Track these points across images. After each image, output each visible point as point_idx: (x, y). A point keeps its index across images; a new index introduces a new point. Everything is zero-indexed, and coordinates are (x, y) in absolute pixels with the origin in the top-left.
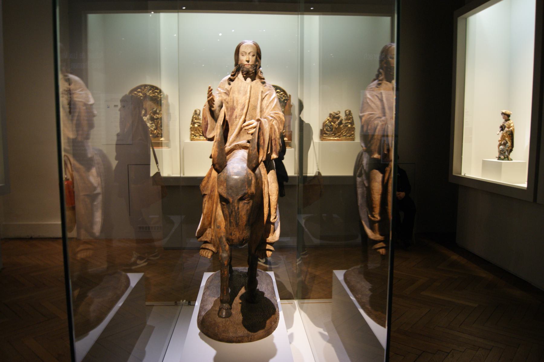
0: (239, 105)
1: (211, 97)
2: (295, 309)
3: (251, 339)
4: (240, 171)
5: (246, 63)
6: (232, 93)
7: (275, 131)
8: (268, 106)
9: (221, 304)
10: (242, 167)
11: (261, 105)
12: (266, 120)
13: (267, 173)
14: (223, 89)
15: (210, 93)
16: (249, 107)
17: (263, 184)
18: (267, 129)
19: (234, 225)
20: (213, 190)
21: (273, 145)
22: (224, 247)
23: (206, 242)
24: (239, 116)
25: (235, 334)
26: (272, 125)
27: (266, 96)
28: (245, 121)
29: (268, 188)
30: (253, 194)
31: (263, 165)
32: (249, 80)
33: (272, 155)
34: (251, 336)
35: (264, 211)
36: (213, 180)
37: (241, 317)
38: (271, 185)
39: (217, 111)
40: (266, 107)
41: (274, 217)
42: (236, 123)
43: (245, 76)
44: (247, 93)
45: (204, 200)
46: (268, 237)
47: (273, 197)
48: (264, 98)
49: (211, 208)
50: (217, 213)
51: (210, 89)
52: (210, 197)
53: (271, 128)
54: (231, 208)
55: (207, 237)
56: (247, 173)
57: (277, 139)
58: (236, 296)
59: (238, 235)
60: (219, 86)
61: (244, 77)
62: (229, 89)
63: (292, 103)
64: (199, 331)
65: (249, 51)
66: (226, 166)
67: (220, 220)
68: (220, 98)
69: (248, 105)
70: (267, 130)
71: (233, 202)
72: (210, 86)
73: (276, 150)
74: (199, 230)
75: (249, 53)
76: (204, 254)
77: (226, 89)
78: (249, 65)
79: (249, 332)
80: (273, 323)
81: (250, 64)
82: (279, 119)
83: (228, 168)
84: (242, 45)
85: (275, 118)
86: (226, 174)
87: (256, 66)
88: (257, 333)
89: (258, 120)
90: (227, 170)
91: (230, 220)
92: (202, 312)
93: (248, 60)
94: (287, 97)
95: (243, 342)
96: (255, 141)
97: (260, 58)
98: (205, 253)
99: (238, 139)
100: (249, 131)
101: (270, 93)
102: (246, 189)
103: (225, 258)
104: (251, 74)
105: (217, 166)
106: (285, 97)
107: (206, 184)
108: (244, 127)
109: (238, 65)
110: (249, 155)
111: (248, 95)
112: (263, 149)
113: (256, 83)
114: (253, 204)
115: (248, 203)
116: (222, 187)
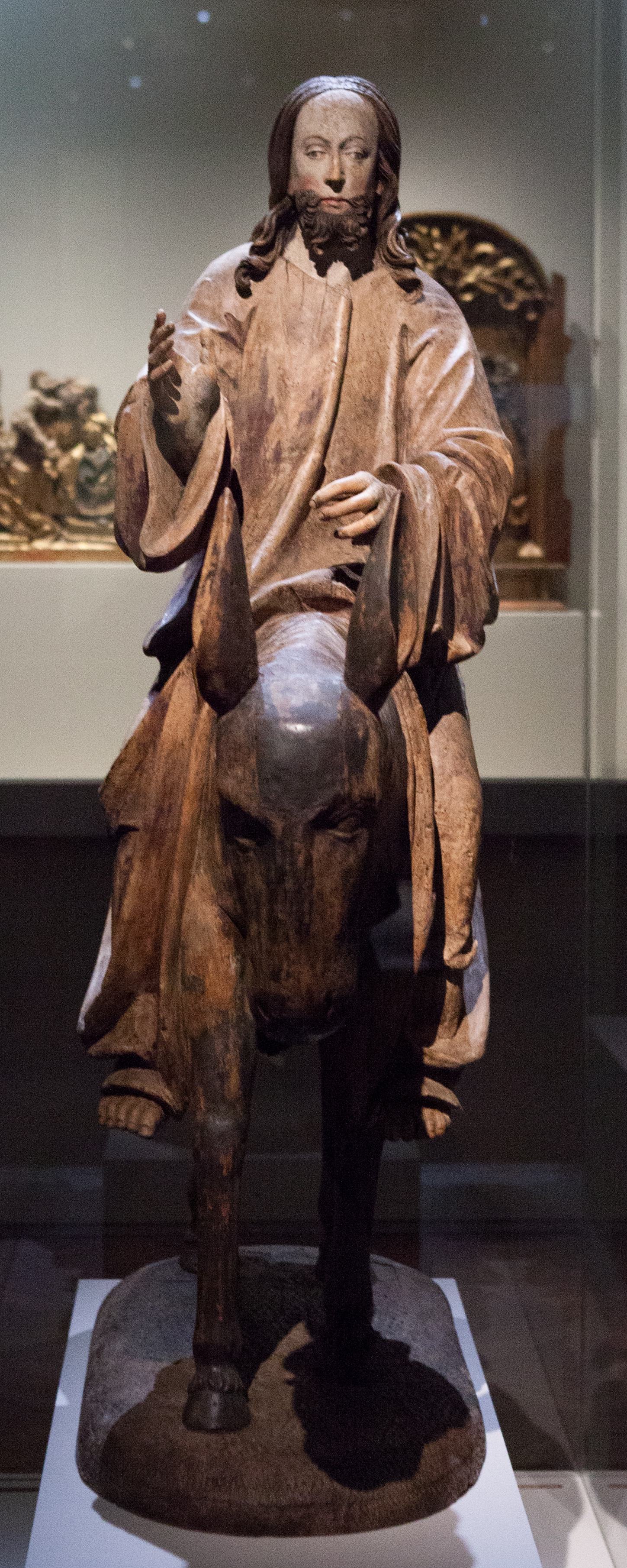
0: (293, 395)
1: (170, 362)
2: (576, 1510)
3: (349, 1517)
4: (316, 701)
5: (328, 192)
6: (259, 334)
7: (467, 522)
8: (434, 399)
9: (198, 1369)
10: (324, 687)
11: (400, 392)
12: (421, 470)
13: (424, 728)
14: (214, 317)
15: (163, 345)
16: (341, 407)
17: (411, 778)
18: (429, 513)
19: (292, 934)
20: (166, 807)
21: (457, 590)
22: (217, 1083)
23: (129, 1061)
24: (292, 450)
25: (272, 1496)
26: (454, 494)
27: (422, 348)
28: (319, 477)
29: (433, 800)
30: (371, 800)
31: (411, 685)
32: (339, 271)
33: (451, 638)
34: (350, 1505)
35: (415, 906)
36: (169, 755)
37: (297, 1431)
38: (447, 787)
39: (192, 429)
40: (422, 406)
41: (462, 943)
42: (276, 481)
43: (320, 252)
44: (333, 339)
45: (122, 858)
46: (430, 1042)
47: (456, 845)
48: (412, 361)
49: (157, 893)
50: (186, 917)
51: (163, 329)
52: (152, 841)
53: (447, 511)
54: (279, 860)
55: (135, 1036)
56: (346, 711)
57: (427, 807)
58: (265, 1354)
59: (306, 978)
60: (190, 299)
61: (313, 256)
62: (242, 317)
63: (574, 326)
64: (92, 1496)
65: (343, 135)
66: (255, 679)
67: (200, 949)
68: (210, 368)
69: (335, 398)
70: (428, 520)
71: (288, 831)
72: (161, 311)
73: (473, 615)
74: (97, 1000)
75: (342, 146)
76: (122, 1117)
77: (227, 315)
78: (340, 200)
79: (338, 1486)
80: (454, 1460)
81: (347, 197)
82: (489, 463)
83: (264, 691)
84: (310, 102)
85: (465, 460)
86: (257, 714)
87: (378, 200)
88: (376, 1493)
89: (389, 474)
90: (260, 699)
91: (271, 911)
92: (102, 1415)
93: (335, 176)
94: (543, 287)
95: (308, 1533)
96: (382, 571)
97: (395, 165)
98: (123, 1110)
99: (289, 561)
100: (342, 524)
101: (441, 338)
102: (343, 781)
103: (222, 1135)
104: (350, 244)
105: (217, 682)
106: (528, 289)
107: (131, 777)
108: (320, 504)
109: (287, 199)
110: (354, 637)
111: (337, 345)
112: (414, 608)
113: (376, 285)
114: (370, 845)
115: (351, 841)
116: (239, 772)
